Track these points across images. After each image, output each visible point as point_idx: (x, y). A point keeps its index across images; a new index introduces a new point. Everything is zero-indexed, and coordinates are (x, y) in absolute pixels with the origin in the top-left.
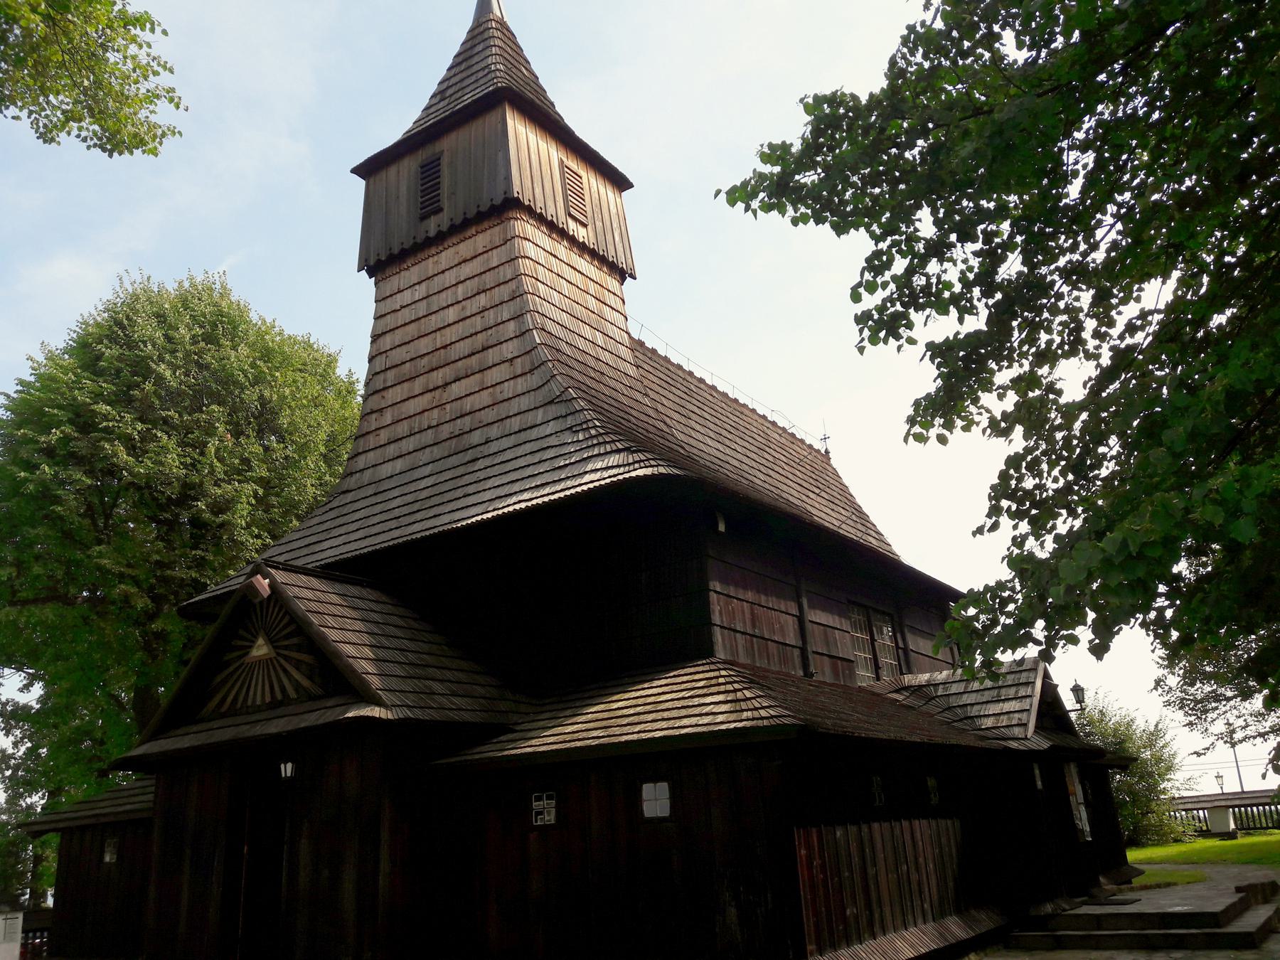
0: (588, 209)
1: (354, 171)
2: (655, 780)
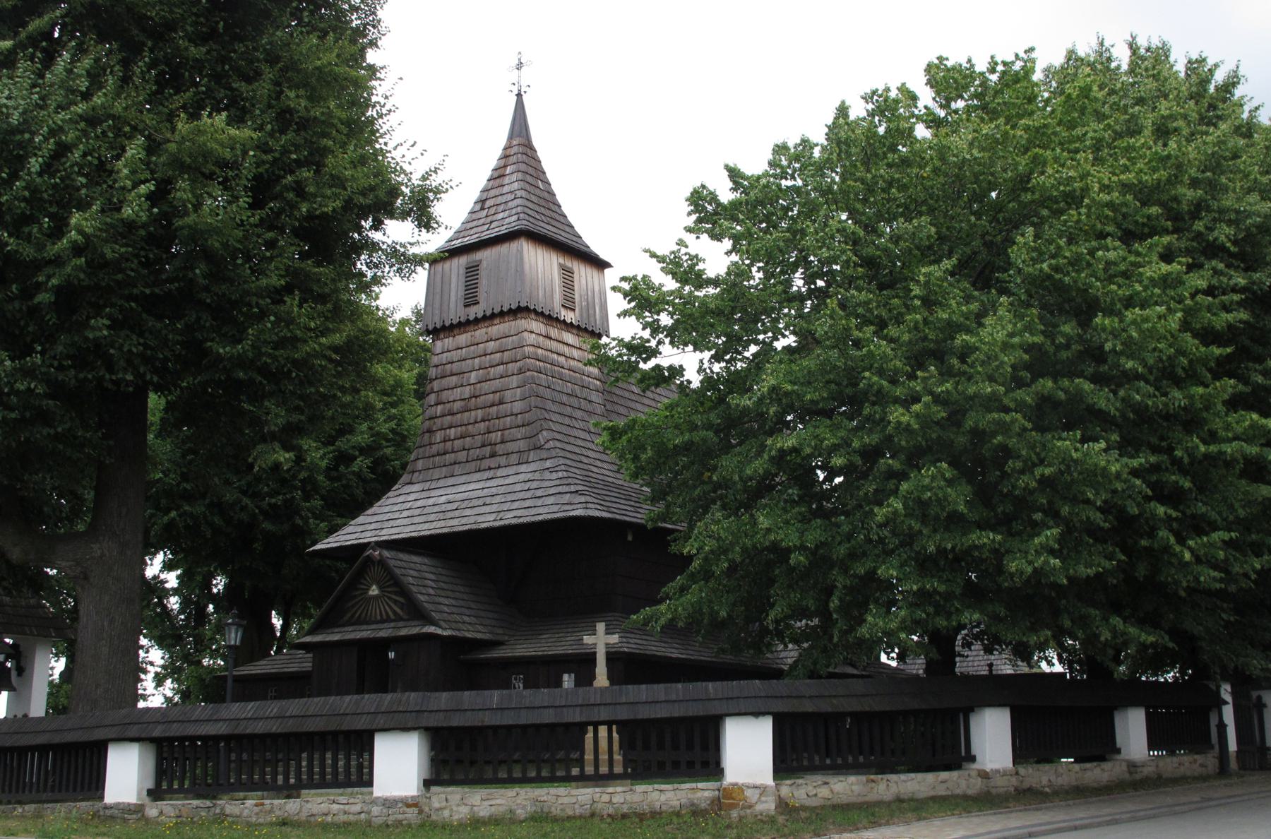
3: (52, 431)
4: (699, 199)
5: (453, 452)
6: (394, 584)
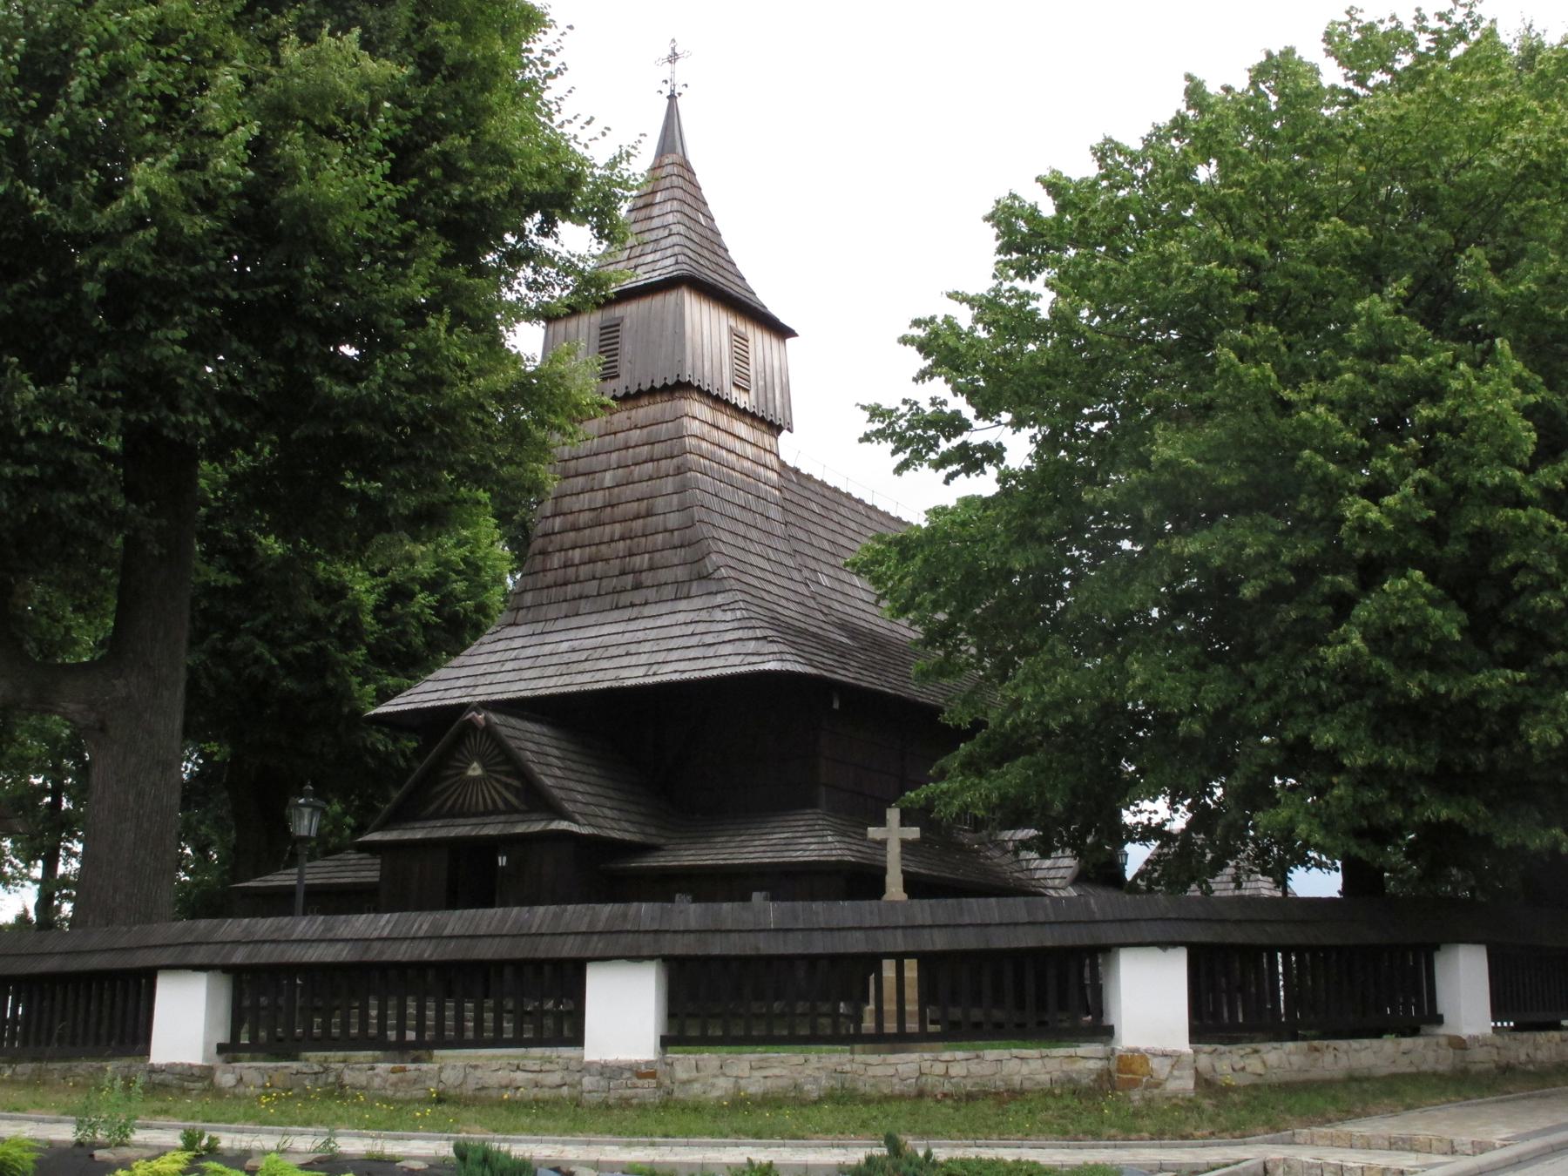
0: (752, 373)
3: (82, 500)
4: (1005, 217)
5: (577, 581)
6: (505, 759)
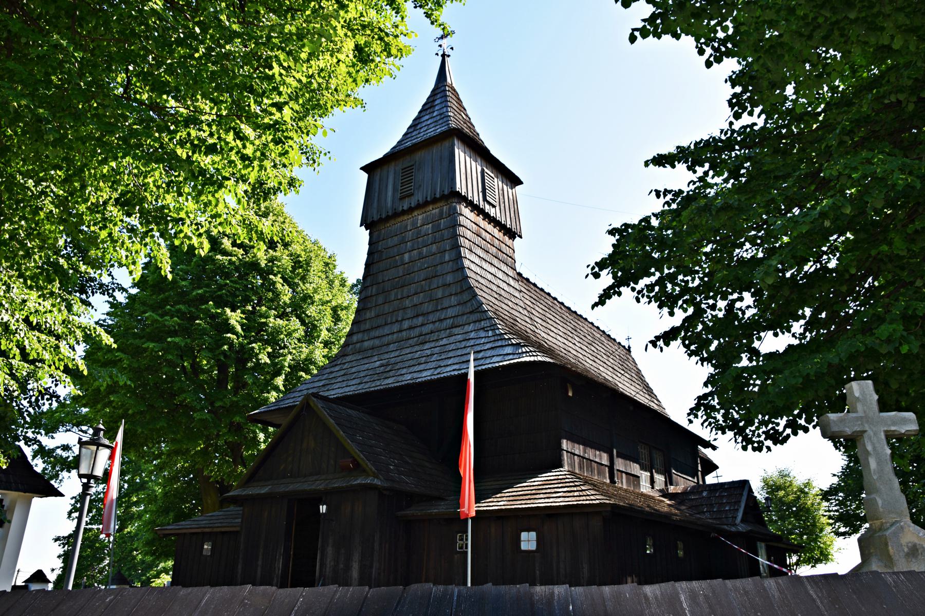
1: (362, 169)
2: (528, 530)
